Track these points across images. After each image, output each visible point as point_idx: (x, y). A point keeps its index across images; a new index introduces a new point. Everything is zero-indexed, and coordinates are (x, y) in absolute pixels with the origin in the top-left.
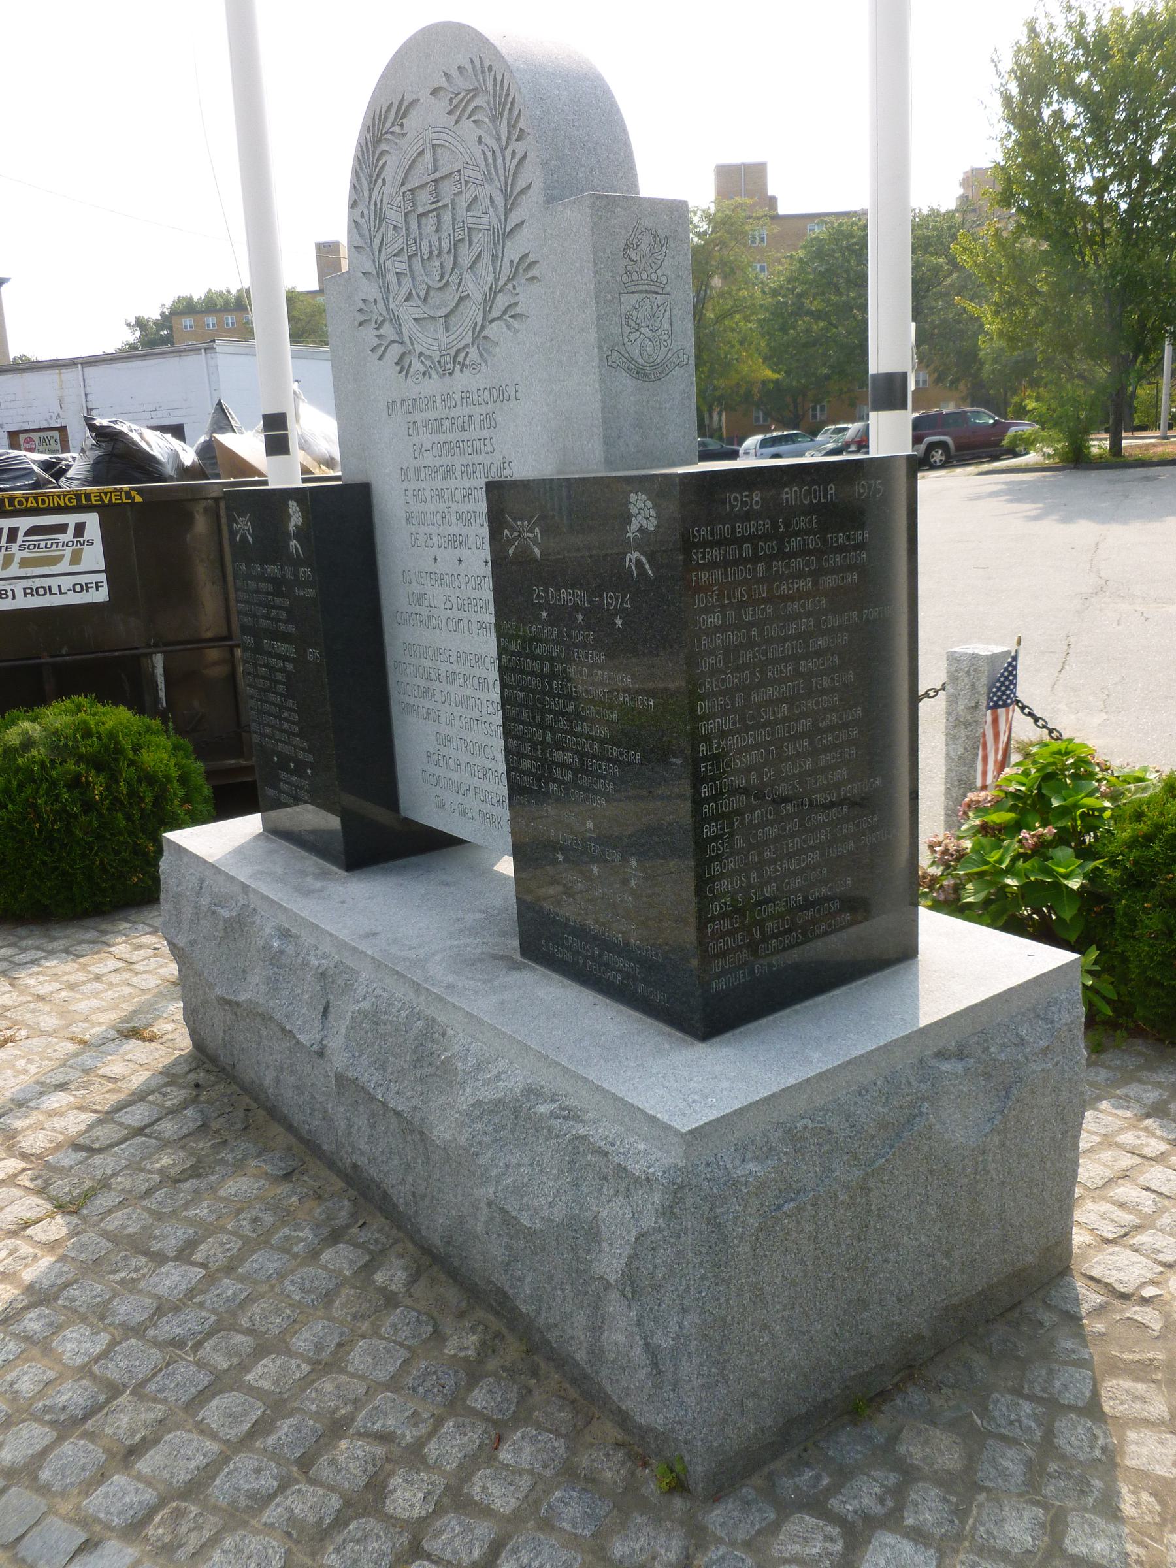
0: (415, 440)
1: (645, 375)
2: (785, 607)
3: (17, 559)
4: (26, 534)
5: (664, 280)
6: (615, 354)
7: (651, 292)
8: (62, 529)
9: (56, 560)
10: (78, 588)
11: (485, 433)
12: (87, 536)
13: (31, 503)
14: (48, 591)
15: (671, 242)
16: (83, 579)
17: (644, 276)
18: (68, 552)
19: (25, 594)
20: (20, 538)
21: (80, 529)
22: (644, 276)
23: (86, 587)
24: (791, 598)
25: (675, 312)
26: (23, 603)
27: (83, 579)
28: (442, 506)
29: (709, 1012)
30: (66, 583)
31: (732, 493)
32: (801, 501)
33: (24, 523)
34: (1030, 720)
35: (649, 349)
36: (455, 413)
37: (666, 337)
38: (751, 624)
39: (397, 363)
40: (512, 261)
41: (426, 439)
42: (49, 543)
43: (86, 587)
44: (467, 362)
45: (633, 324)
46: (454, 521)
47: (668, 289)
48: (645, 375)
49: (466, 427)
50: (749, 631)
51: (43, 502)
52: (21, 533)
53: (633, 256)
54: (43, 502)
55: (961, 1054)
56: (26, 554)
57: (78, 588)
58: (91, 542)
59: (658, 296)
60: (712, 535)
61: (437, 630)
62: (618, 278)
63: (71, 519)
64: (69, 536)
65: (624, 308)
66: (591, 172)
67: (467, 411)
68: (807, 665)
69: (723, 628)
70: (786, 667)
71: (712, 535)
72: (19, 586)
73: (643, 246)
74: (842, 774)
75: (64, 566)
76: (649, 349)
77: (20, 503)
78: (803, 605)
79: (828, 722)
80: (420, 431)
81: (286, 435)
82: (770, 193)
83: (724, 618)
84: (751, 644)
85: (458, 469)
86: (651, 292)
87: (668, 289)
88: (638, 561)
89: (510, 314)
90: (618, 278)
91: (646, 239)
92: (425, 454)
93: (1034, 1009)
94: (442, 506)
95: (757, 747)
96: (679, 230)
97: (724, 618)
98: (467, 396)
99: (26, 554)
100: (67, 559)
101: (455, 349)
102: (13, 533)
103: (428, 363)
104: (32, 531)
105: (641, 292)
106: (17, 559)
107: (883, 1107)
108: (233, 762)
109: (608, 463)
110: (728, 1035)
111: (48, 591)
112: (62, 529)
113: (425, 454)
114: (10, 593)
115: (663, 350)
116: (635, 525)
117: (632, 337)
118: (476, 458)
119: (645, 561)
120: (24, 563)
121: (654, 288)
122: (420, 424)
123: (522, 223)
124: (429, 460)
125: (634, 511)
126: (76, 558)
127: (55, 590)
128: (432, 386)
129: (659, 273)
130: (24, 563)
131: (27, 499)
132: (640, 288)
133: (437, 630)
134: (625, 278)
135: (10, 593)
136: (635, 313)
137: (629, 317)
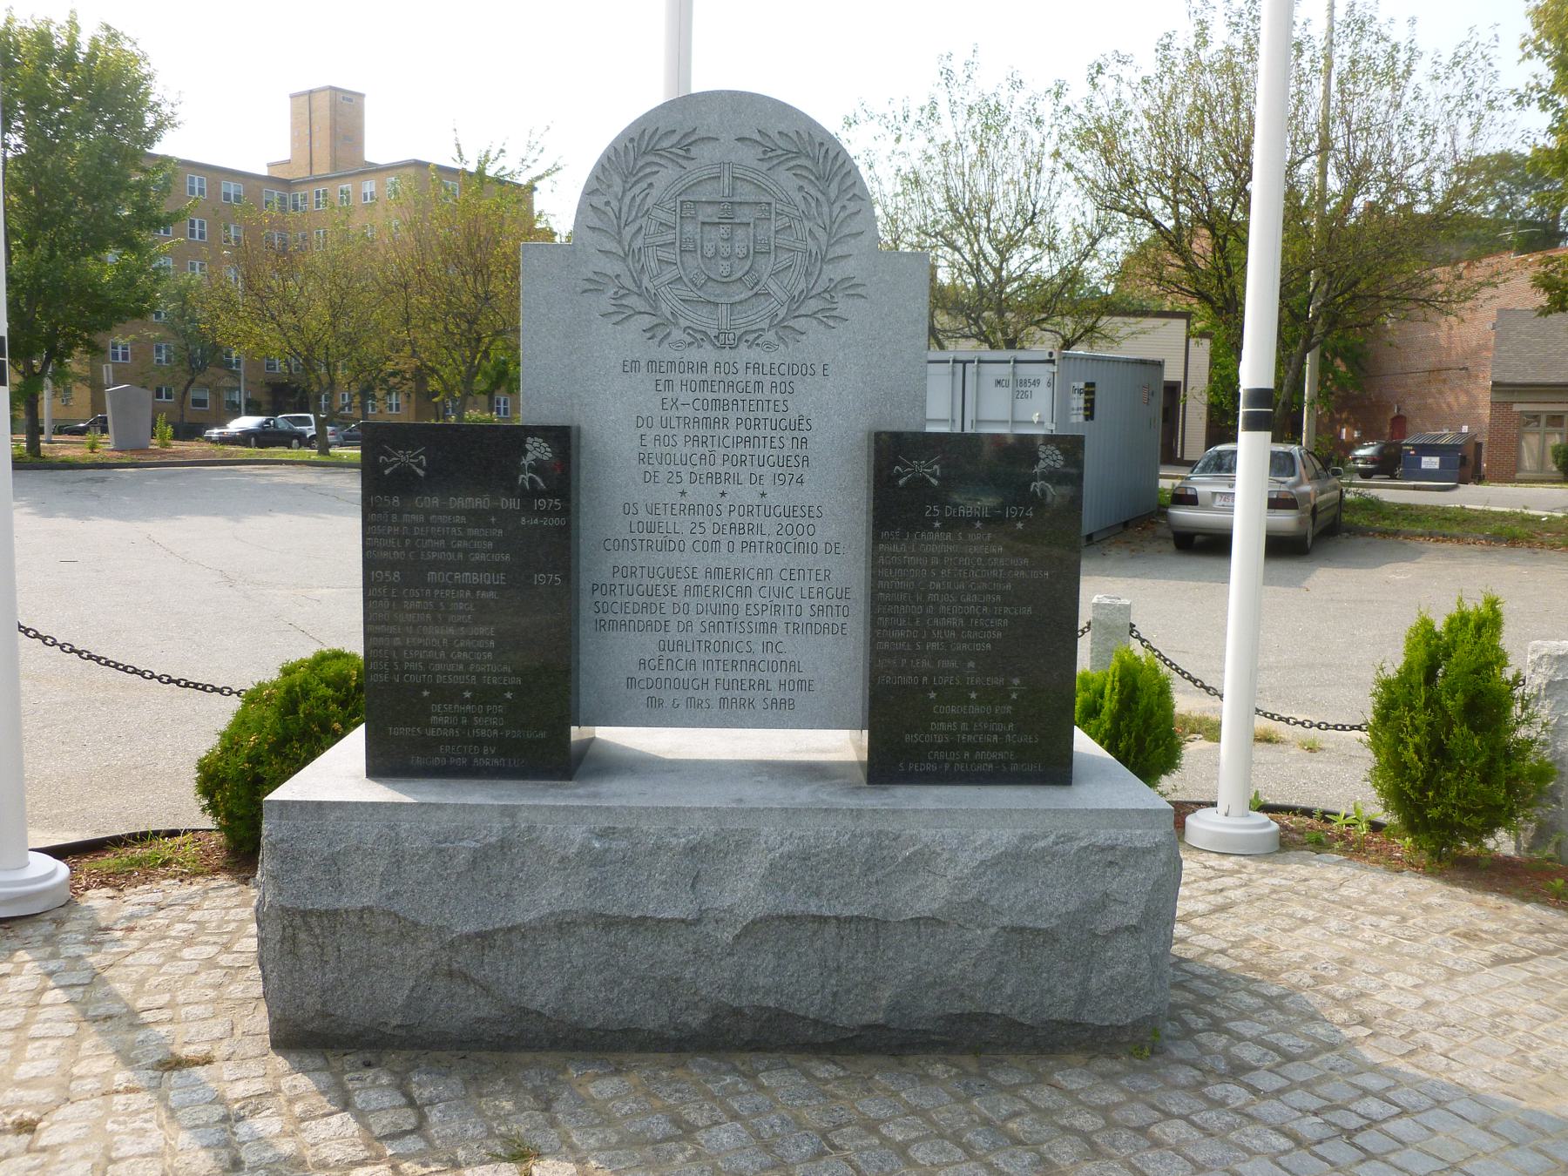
41: (685, 396)
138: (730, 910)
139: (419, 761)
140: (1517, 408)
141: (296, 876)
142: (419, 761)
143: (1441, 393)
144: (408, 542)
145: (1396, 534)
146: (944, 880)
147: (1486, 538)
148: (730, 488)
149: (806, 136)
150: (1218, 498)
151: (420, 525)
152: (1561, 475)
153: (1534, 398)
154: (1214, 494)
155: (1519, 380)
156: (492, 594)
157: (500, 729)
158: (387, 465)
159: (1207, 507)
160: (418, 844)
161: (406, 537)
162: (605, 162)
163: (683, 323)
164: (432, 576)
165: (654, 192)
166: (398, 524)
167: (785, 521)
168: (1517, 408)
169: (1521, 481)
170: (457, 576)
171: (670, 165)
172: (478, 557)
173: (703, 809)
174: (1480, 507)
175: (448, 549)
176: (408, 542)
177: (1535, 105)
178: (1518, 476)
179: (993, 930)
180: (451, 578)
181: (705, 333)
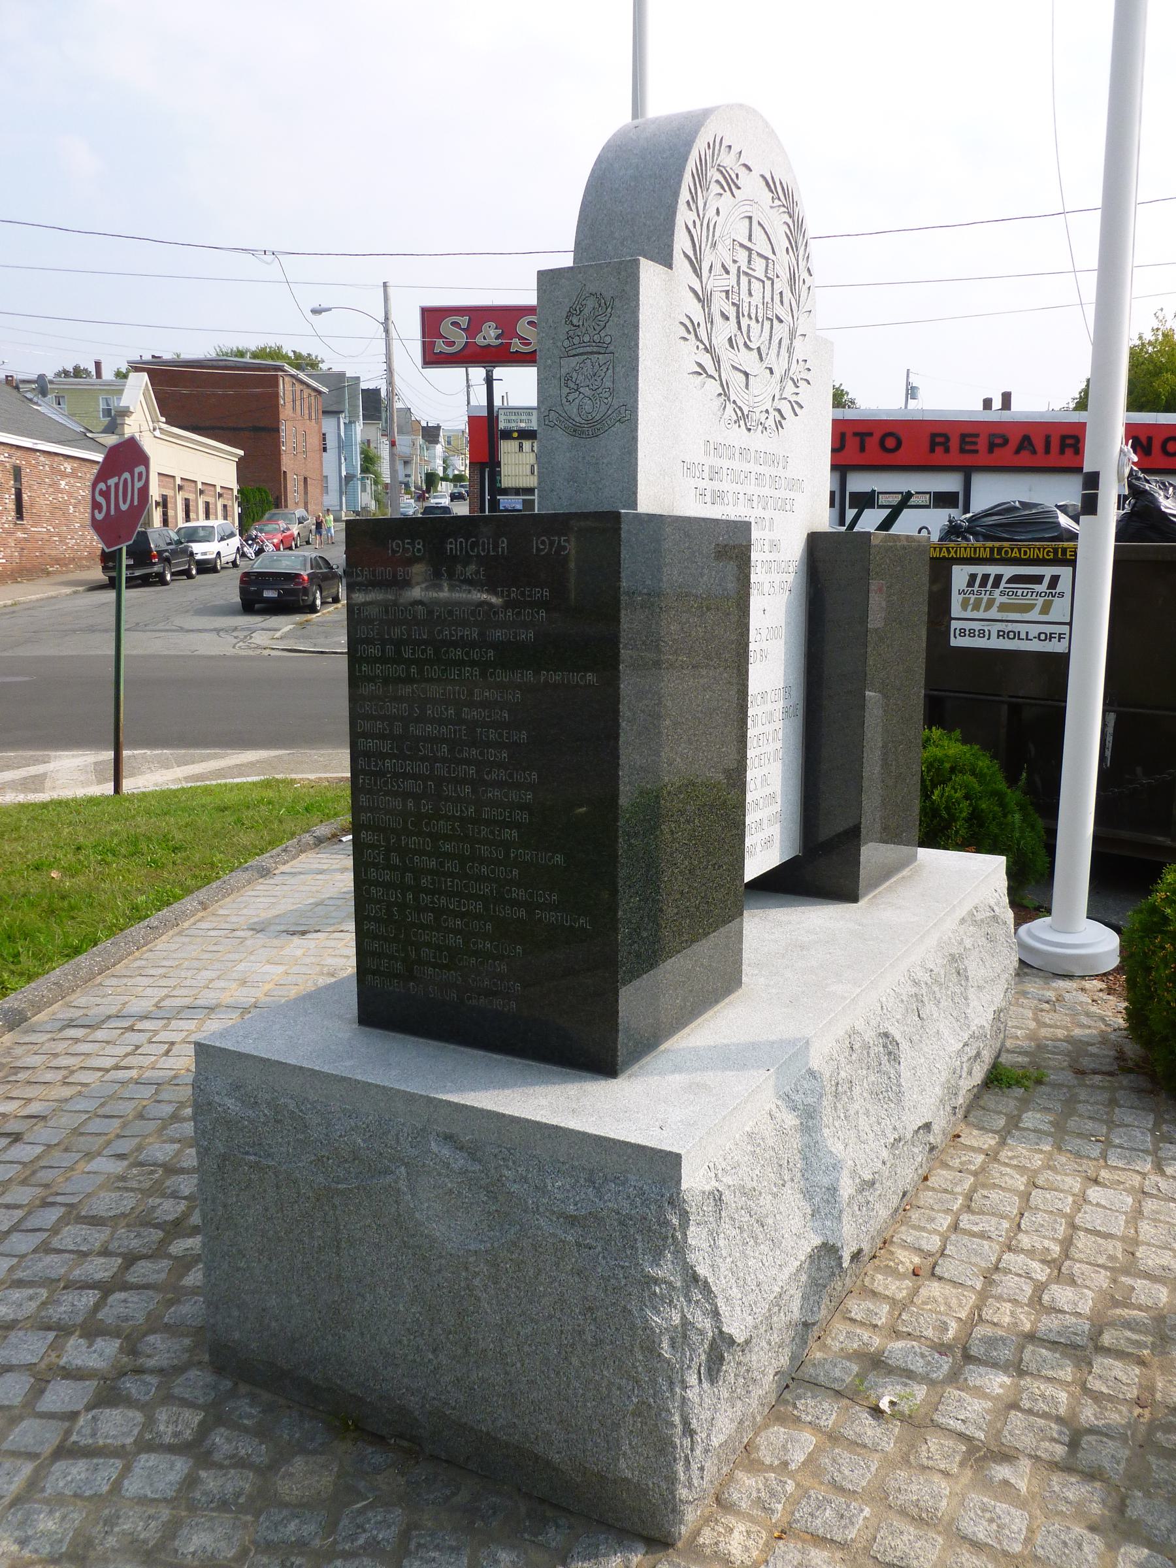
1: (583, 432)
2: (447, 652)
3: (997, 604)
4: (1008, 582)
5: (608, 339)
6: (552, 413)
7: (592, 353)
8: (1038, 579)
9: (1028, 608)
10: (1043, 637)
12: (1058, 590)
13: (1015, 554)
14: (1017, 635)
15: (617, 303)
16: (1048, 629)
17: (587, 338)
18: (1040, 601)
19: (999, 636)
20: (1003, 584)
21: (1055, 580)
22: (587, 338)
23: (1050, 637)
24: (455, 644)
25: (617, 369)
26: (995, 643)
27: (1048, 629)
30: (1034, 630)
31: (393, 540)
32: (467, 552)
33: (1009, 571)
35: (588, 408)
37: (607, 395)
38: (410, 662)
40: (781, 321)
42: (1020, 591)
43: (1050, 637)
45: (572, 385)
47: (611, 348)
48: (583, 432)
50: (408, 669)
51: (1025, 553)
52: (1004, 580)
53: (575, 321)
54: (1025, 553)
55: (473, 1152)
56: (1004, 599)
57: (1043, 637)
58: (1061, 595)
59: (600, 356)
60: (374, 575)
62: (559, 344)
63: (1048, 572)
64: (1043, 587)
65: (563, 371)
66: (622, 244)
68: (469, 714)
69: (383, 660)
70: (446, 709)
71: (374, 575)
72: (995, 628)
73: (586, 311)
74: (512, 834)
75: (1034, 615)
76: (588, 408)
77: (1006, 552)
78: (467, 654)
79: (494, 776)
81: (1096, 495)
83: (383, 651)
84: (409, 680)
86: (592, 353)
87: (611, 348)
90: (559, 344)
91: (591, 303)
93: (592, 1171)
95: (415, 777)
96: (627, 288)
97: (383, 651)
99: (1004, 599)
100: (1038, 609)
102: (998, 578)
104: (1015, 579)
105: (582, 354)
106: (997, 604)
107: (364, 1141)
108: (1160, 839)
111: (1017, 635)
112: (1038, 579)
114: (987, 633)
115: (604, 408)
117: (570, 398)
120: (1003, 608)
121: (595, 349)
123: (690, 288)
126: (1046, 609)
127: (1023, 636)
129: (603, 334)
130: (1003, 608)
131: (1012, 549)
132: (581, 350)
134: (566, 343)
135: (987, 633)
136: (575, 375)
137: (568, 378)
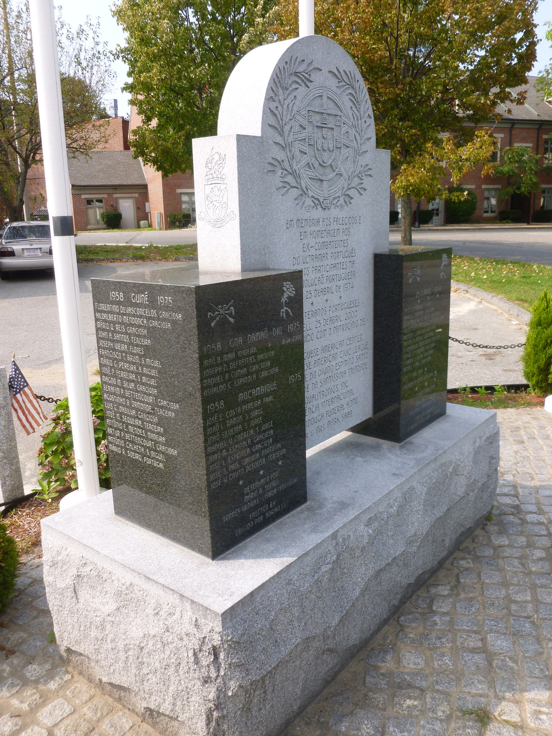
0: (305, 241)
11: (345, 238)
28: (319, 275)
29: (225, 540)
34: (459, 339)
36: (331, 228)
39: (295, 199)
41: (312, 242)
44: (338, 204)
46: (325, 281)
49: (335, 234)
61: (311, 341)
67: (337, 227)
80: (309, 237)
82: (160, 172)
85: (330, 255)
88: (286, 310)
89: (286, 189)
92: (310, 249)
94: (319, 275)
98: (336, 220)
101: (332, 197)
103: (316, 202)
109: (244, 269)
110: (251, 542)
113: (310, 249)
116: (285, 296)
118: (339, 249)
119: (289, 310)
122: (309, 233)
124: (313, 252)
125: (284, 289)
128: (318, 213)
133: (311, 341)
138: (415, 535)
139: (239, 531)
140: (83, 196)
141: (255, 654)
142: (239, 531)
143: (38, 189)
144: (227, 376)
145: (92, 260)
146: (463, 477)
147: (132, 258)
148: (328, 296)
149: (353, 75)
150: (25, 251)
151: (234, 360)
152: (105, 226)
153: (90, 192)
154: (23, 249)
155: (83, 184)
156: (270, 398)
157: (277, 487)
158: (213, 319)
159: (20, 257)
160: (307, 585)
161: (226, 372)
162: (275, 77)
163: (310, 193)
164: (242, 396)
165: (297, 102)
166: (221, 364)
167: (348, 311)
168: (83, 196)
169: (90, 230)
170: (254, 391)
171: (303, 85)
172: (264, 374)
173: (396, 487)
174: (115, 244)
175: (249, 373)
176: (227, 376)
177: (121, 58)
178: (89, 227)
179: (476, 491)
180: (251, 394)
181: (318, 200)
